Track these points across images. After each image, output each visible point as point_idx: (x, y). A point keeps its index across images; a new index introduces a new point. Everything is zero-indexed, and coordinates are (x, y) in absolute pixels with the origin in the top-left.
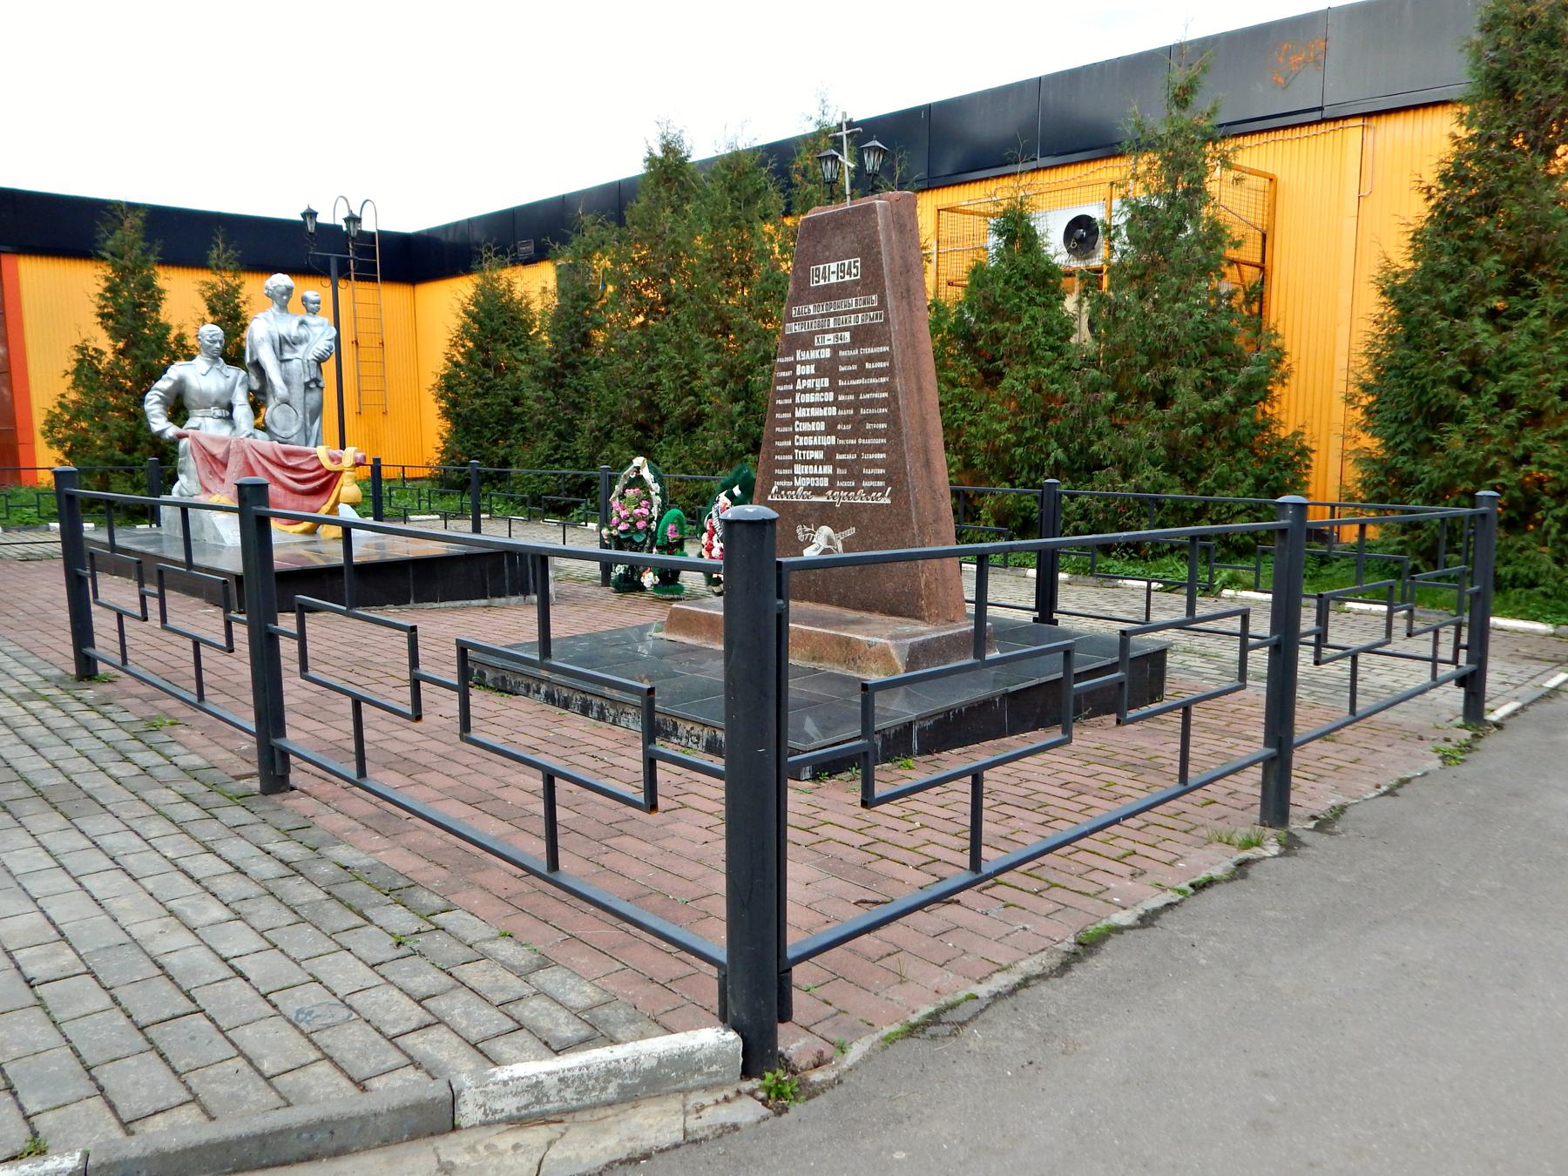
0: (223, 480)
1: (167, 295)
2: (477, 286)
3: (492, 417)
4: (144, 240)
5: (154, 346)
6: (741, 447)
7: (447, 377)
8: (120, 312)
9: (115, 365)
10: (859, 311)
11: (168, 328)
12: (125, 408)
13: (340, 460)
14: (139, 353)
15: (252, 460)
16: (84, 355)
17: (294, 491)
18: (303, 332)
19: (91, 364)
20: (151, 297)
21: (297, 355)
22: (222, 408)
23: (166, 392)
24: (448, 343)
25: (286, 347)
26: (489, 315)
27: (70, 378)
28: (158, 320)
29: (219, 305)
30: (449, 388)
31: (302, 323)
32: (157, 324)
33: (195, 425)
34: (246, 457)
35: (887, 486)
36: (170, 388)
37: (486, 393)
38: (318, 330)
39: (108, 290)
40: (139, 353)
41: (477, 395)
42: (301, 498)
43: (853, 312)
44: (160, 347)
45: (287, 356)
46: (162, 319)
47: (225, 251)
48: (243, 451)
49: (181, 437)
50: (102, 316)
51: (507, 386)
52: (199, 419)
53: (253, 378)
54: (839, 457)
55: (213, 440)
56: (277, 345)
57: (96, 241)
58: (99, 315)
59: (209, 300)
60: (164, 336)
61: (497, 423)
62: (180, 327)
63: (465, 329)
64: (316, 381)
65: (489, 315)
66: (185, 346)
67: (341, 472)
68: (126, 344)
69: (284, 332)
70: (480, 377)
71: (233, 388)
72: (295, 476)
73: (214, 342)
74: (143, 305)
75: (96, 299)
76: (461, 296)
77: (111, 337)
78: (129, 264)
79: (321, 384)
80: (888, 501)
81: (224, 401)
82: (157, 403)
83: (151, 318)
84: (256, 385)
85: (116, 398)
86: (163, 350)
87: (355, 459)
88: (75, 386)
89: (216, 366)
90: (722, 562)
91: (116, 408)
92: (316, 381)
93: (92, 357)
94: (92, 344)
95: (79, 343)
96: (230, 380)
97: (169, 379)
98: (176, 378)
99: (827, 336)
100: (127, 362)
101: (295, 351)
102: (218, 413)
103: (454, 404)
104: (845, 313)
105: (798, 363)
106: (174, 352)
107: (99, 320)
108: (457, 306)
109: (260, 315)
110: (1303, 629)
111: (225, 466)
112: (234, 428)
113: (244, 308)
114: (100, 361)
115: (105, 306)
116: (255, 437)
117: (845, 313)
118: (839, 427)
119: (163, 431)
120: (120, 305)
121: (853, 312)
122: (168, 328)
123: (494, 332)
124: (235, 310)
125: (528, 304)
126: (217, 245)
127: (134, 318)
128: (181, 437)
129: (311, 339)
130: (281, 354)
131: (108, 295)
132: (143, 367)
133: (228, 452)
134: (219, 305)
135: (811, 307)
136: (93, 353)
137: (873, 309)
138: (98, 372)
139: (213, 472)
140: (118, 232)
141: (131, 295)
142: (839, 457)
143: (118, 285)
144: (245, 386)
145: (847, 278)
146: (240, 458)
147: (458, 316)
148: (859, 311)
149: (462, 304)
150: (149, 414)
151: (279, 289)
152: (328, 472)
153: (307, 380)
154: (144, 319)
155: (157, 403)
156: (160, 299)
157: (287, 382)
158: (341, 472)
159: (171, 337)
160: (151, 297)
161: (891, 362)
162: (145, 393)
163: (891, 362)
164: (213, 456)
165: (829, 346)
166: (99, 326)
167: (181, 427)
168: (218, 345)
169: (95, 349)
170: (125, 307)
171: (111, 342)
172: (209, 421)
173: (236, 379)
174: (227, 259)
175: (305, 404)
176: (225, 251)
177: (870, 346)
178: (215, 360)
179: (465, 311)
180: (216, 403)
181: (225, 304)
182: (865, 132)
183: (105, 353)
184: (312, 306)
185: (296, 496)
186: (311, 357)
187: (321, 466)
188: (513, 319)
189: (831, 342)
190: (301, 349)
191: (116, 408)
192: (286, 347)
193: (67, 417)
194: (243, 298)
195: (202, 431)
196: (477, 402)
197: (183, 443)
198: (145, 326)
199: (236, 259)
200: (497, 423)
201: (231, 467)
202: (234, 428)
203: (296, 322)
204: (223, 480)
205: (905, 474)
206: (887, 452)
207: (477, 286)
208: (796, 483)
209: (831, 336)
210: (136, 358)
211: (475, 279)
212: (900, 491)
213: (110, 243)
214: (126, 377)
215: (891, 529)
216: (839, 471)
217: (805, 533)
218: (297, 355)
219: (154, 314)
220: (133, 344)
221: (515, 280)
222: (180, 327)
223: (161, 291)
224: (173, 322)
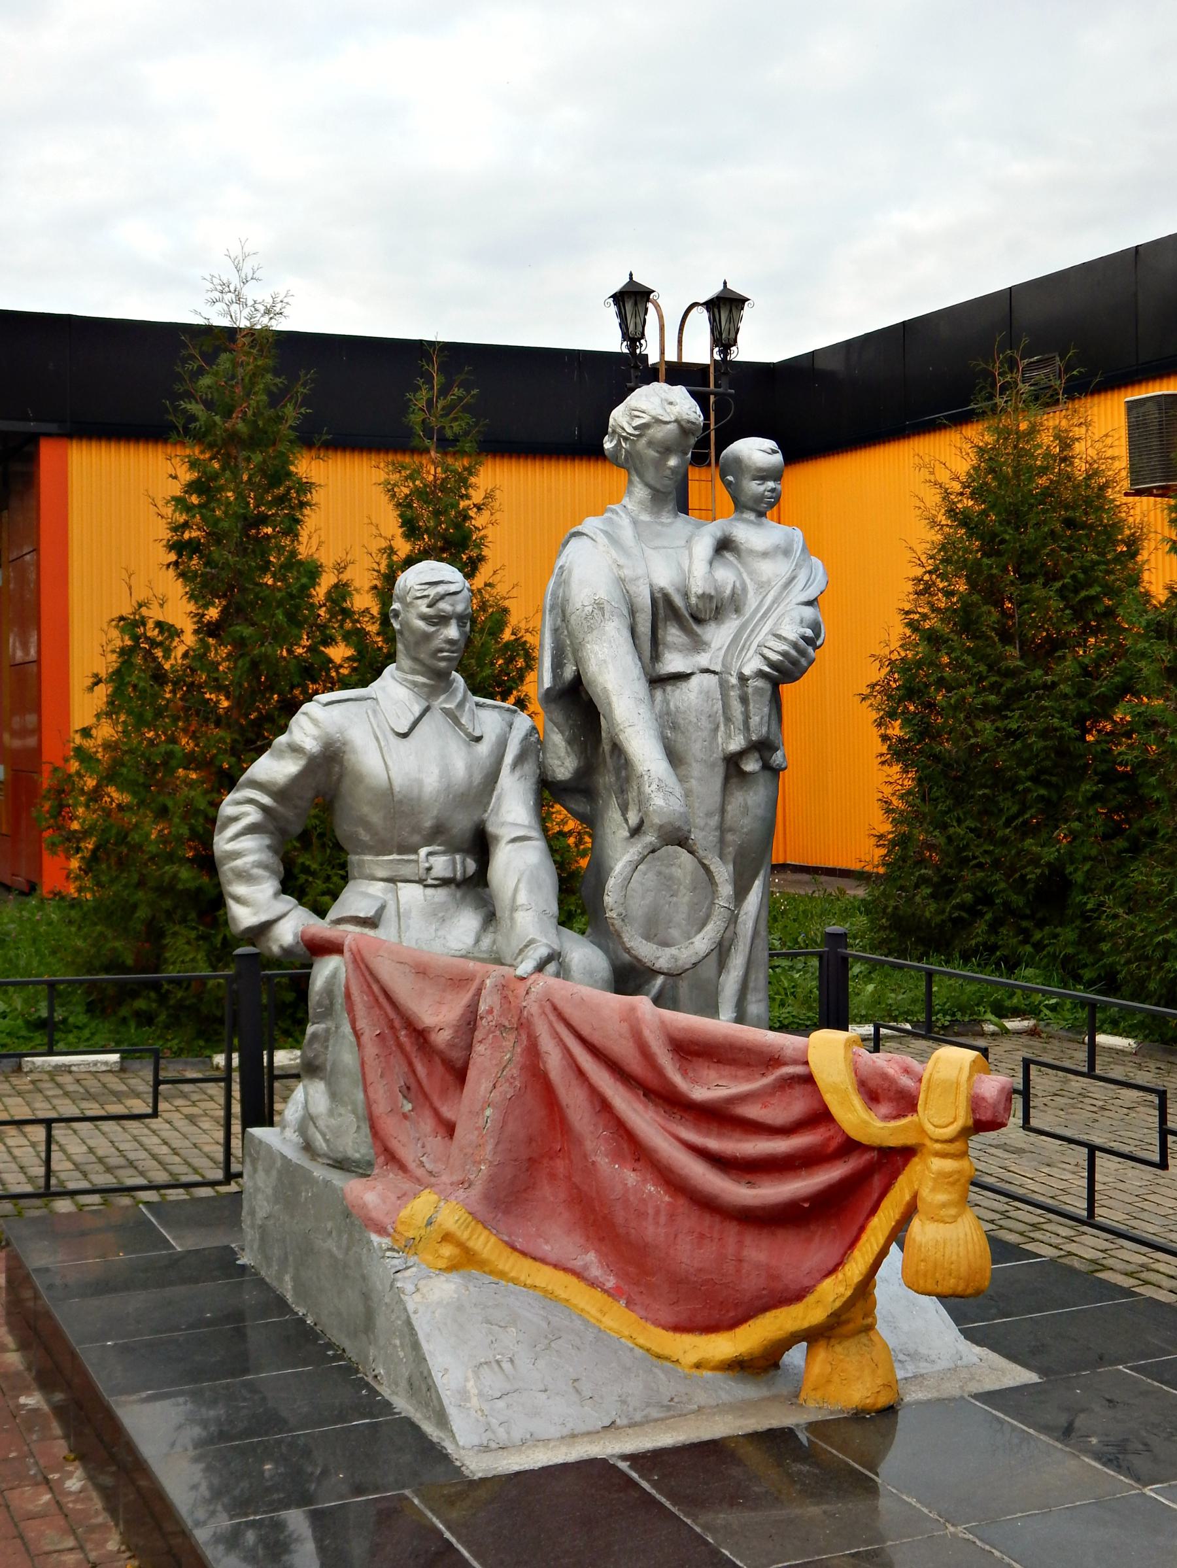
0: (449, 1129)
1: (315, 496)
2: (981, 451)
3: (1025, 764)
4: (277, 372)
5: (280, 616)
7: (904, 667)
8: (216, 537)
9: (198, 658)
11: (313, 572)
12: (211, 763)
13: (906, 1103)
14: (247, 631)
15: (554, 1063)
16: (136, 638)
17: (707, 1204)
18: (726, 576)
19: (148, 654)
20: (281, 500)
21: (703, 660)
22: (452, 848)
23: (282, 794)
24: (910, 587)
25: (673, 634)
26: (1015, 517)
27: (103, 691)
28: (294, 553)
29: (425, 515)
30: (911, 692)
31: (724, 546)
32: (292, 562)
33: (365, 910)
34: (533, 1051)
36: (296, 780)
37: (1006, 705)
38: (773, 570)
39: (193, 487)
40: (247, 631)
41: (987, 711)
42: (732, 1229)
44: (294, 619)
45: (673, 663)
46: (304, 551)
47: (444, 391)
48: (523, 1025)
49: (319, 948)
50: (178, 547)
51: (1065, 688)
52: (377, 889)
53: (557, 740)
55: (422, 971)
56: (644, 627)
57: (179, 378)
58: (173, 546)
59: (404, 506)
60: (305, 591)
61: (1034, 779)
62: (340, 568)
63: (947, 556)
64: (763, 747)
65: (1015, 517)
66: (347, 613)
67: (907, 1153)
68: (224, 612)
69: (664, 578)
70: (990, 667)
71: (492, 778)
72: (713, 1144)
73: (442, 620)
74: (263, 520)
75: (169, 511)
76: (943, 476)
77: (192, 597)
78: (241, 427)
79: (777, 758)
81: (462, 823)
82: (252, 829)
83: (280, 549)
84: (564, 765)
85: (194, 737)
86: (299, 625)
87: (976, 1102)
88: (112, 709)
89: (441, 702)
91: (190, 761)
92: (763, 747)
93: (153, 643)
94: (154, 613)
95: (126, 611)
96: (484, 749)
97: (295, 749)
98: (311, 745)
100: (224, 651)
101: (698, 645)
102: (441, 865)
103: (924, 731)
106: (324, 627)
107: (172, 557)
108: (933, 498)
109: (591, 524)
111: (460, 1074)
112: (490, 918)
113: (479, 520)
114: (168, 652)
115: (185, 525)
116: (563, 972)
119: (266, 927)
120: (218, 521)
122: (313, 572)
123: (1026, 557)
124: (458, 526)
125: (1103, 488)
126: (429, 380)
127: (241, 550)
128: (319, 948)
129: (752, 601)
130: (656, 656)
131: (195, 499)
132: (255, 665)
133: (470, 1021)
134: (425, 515)
136: (153, 633)
138: (159, 677)
139: (414, 1090)
140: (224, 356)
141: (241, 497)
143: (215, 477)
144: (530, 768)
146: (511, 1050)
147: (933, 523)
149: (946, 494)
150: (226, 869)
151: (658, 433)
152: (850, 1146)
153: (736, 744)
154: (264, 554)
155: (252, 829)
156: (302, 505)
157: (674, 756)
158: (907, 1153)
159: (320, 592)
160: (281, 500)
162: (206, 841)
164: (421, 1035)
166: (171, 572)
167: (321, 913)
168: (452, 632)
169: (159, 624)
170: (225, 525)
171: (191, 607)
172: (411, 893)
173: (502, 744)
174: (448, 410)
175: (722, 829)
176: (444, 391)
178: (439, 681)
179: (951, 512)
180: (437, 834)
181: (437, 513)
183: (179, 633)
184: (755, 487)
185: (708, 1221)
186: (752, 665)
187: (821, 1116)
188: (1069, 523)
190: (719, 635)
191: (190, 761)
192: (673, 634)
193: (90, 783)
194: (477, 497)
195: (386, 933)
196: (986, 727)
197: (326, 970)
198: (265, 567)
199: (467, 409)
200: (1034, 779)
201: (479, 1083)
202: (490, 918)
203: (704, 546)
204: (449, 1129)
207: (981, 451)
210: (240, 644)
211: (977, 434)
213: (206, 381)
214: (219, 688)
218: (703, 660)
219: (286, 541)
220: (239, 610)
221: (1078, 432)
222: (340, 568)
223: (306, 487)
224: (327, 558)
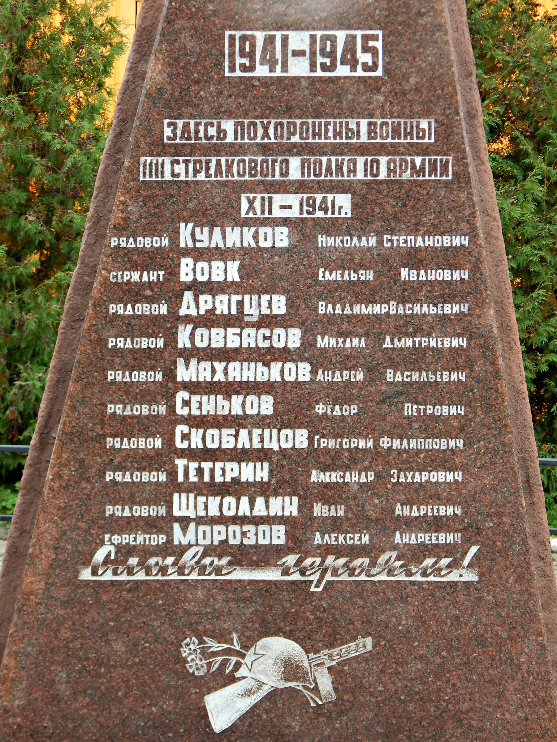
6: (290, 288)
10: (382, 149)
35: (467, 542)
43: (362, 150)
54: (316, 476)
80: (471, 576)
90: (168, 176)
99: (278, 199)
104: (336, 150)
105: (186, 252)
110: (328, 480)
117: (336, 150)
118: (320, 409)
121: (362, 150)
135: (228, 125)
137: (424, 150)
142: (316, 476)
145: (342, 71)
148: (382, 149)
161: (475, 269)
163: (475, 269)
165: (285, 222)
177: (415, 230)
182: (255, 42)
189: (294, 213)
205: (519, 517)
206: (464, 469)
208: (178, 536)
209: (293, 199)
212: (504, 553)
215: (480, 640)
216: (318, 510)
217: (206, 654)
